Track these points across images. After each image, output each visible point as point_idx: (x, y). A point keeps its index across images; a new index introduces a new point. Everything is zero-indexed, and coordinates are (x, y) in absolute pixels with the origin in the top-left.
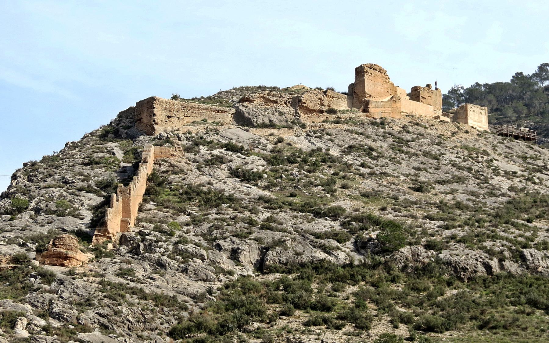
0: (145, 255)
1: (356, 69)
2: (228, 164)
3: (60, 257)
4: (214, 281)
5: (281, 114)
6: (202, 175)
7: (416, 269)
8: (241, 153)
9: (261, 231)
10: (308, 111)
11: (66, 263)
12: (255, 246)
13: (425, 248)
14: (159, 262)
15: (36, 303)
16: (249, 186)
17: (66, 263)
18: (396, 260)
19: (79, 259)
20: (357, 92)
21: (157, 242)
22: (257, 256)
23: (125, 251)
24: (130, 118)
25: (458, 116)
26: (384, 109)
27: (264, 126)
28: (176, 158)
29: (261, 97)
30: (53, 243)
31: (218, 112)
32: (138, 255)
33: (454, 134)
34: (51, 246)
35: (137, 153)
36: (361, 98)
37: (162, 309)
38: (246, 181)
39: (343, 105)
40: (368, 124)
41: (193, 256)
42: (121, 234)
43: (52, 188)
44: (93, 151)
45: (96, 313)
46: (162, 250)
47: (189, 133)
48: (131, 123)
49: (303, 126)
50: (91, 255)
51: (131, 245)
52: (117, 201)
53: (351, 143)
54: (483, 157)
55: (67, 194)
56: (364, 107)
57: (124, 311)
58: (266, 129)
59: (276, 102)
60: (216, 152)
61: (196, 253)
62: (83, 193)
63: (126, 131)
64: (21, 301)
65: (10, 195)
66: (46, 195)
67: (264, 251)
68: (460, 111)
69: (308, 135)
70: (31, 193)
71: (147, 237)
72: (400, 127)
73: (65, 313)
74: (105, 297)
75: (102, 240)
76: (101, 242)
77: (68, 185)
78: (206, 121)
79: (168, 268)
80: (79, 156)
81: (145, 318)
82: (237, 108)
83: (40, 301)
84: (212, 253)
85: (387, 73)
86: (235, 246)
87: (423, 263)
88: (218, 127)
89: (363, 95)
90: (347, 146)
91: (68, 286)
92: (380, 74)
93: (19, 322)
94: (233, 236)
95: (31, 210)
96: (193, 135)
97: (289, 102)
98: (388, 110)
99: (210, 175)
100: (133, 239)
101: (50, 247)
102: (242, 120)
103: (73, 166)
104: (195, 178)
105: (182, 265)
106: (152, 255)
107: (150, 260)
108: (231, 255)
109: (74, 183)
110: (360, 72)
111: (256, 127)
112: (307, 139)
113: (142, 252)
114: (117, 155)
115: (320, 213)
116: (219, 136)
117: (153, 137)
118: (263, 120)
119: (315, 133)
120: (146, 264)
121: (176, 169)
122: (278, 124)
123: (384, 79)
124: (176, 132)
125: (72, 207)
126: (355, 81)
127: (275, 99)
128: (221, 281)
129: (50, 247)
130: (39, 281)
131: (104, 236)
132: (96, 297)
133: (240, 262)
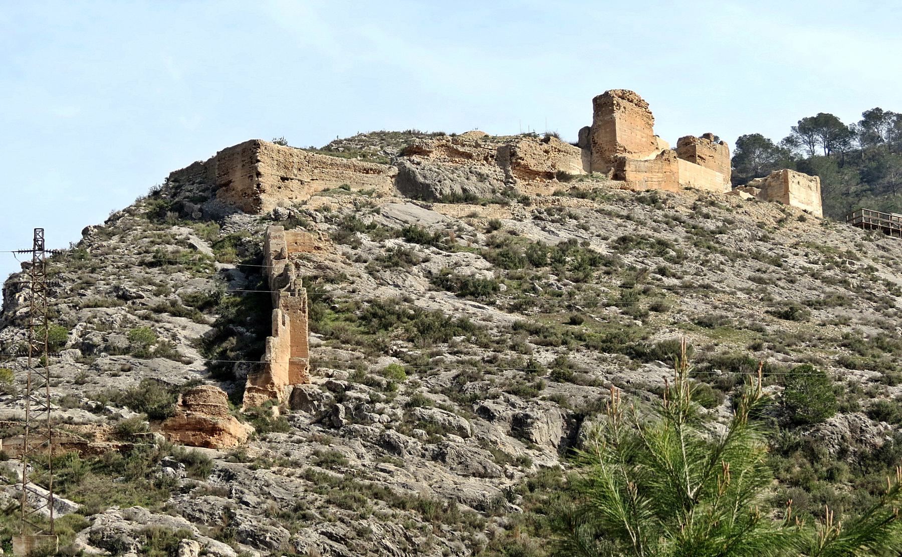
0: (352, 427)
1: (595, 100)
2: (423, 265)
3: (200, 430)
4: (499, 477)
5: (482, 177)
6: (382, 285)
7: (862, 457)
8: (437, 247)
9: (554, 384)
10: (529, 174)
11: (212, 440)
12: (556, 411)
13: (872, 418)
14: (385, 441)
15: (197, 515)
16: (477, 304)
17: (212, 440)
18: (823, 439)
19: (233, 434)
20: (600, 142)
21: (372, 402)
22: (560, 431)
23: (307, 421)
24: (200, 183)
25: (769, 191)
26: (650, 175)
27: (454, 199)
28: (325, 254)
29: (443, 146)
30: (184, 402)
31: (367, 173)
32: (338, 428)
33: (780, 222)
34: (180, 409)
35: (242, 244)
36: (607, 153)
37: (439, 527)
38: (472, 298)
39: (576, 166)
40: (631, 200)
41: (447, 429)
42: (291, 387)
43: (102, 306)
44: (152, 242)
45: (322, 533)
46: (385, 417)
47: (327, 209)
48: (204, 191)
49: (525, 201)
50: (249, 428)
51: (316, 410)
52: (284, 324)
53: (621, 233)
54: (854, 264)
55: (134, 317)
56: (616, 171)
57: (374, 528)
58: (461, 206)
59: (469, 156)
60: (390, 243)
61: (450, 423)
62: (165, 315)
63: (199, 206)
64: (165, 509)
65: (19, 321)
66: (95, 320)
67: (574, 422)
68: (773, 184)
69: (536, 218)
70: (63, 316)
71: (348, 393)
72: (686, 207)
73: (267, 531)
74: (329, 502)
75: (261, 398)
76: (258, 402)
77: (130, 302)
78: (349, 189)
79: (404, 451)
80: (125, 249)
81: (413, 544)
82: (400, 165)
83: (204, 509)
84: (476, 424)
85: (650, 109)
86: (517, 411)
87: (874, 446)
88: (373, 200)
89: (611, 148)
90: (616, 238)
91: (247, 482)
92: (637, 109)
93: (186, 549)
94: (509, 393)
95: (73, 347)
96: (334, 212)
97: (492, 156)
98: (657, 176)
99: (397, 286)
100: (314, 396)
101: (179, 409)
102: (412, 188)
103: (127, 267)
104: (369, 289)
105: (431, 446)
106: (369, 428)
107: (365, 437)
108: (513, 429)
109: (142, 297)
110: (604, 105)
111: (440, 201)
112: (538, 225)
113: (344, 421)
114: (199, 248)
115: (644, 354)
116: (381, 216)
117: (258, 217)
118: (452, 189)
119: (550, 214)
120: (358, 444)
121: (332, 275)
122: (478, 195)
123: (645, 119)
124: (304, 207)
125: (157, 342)
126: (595, 122)
127: (466, 149)
128: (511, 477)
129: (179, 409)
130: (181, 472)
131: (264, 391)
132: (312, 503)
133: (532, 441)
